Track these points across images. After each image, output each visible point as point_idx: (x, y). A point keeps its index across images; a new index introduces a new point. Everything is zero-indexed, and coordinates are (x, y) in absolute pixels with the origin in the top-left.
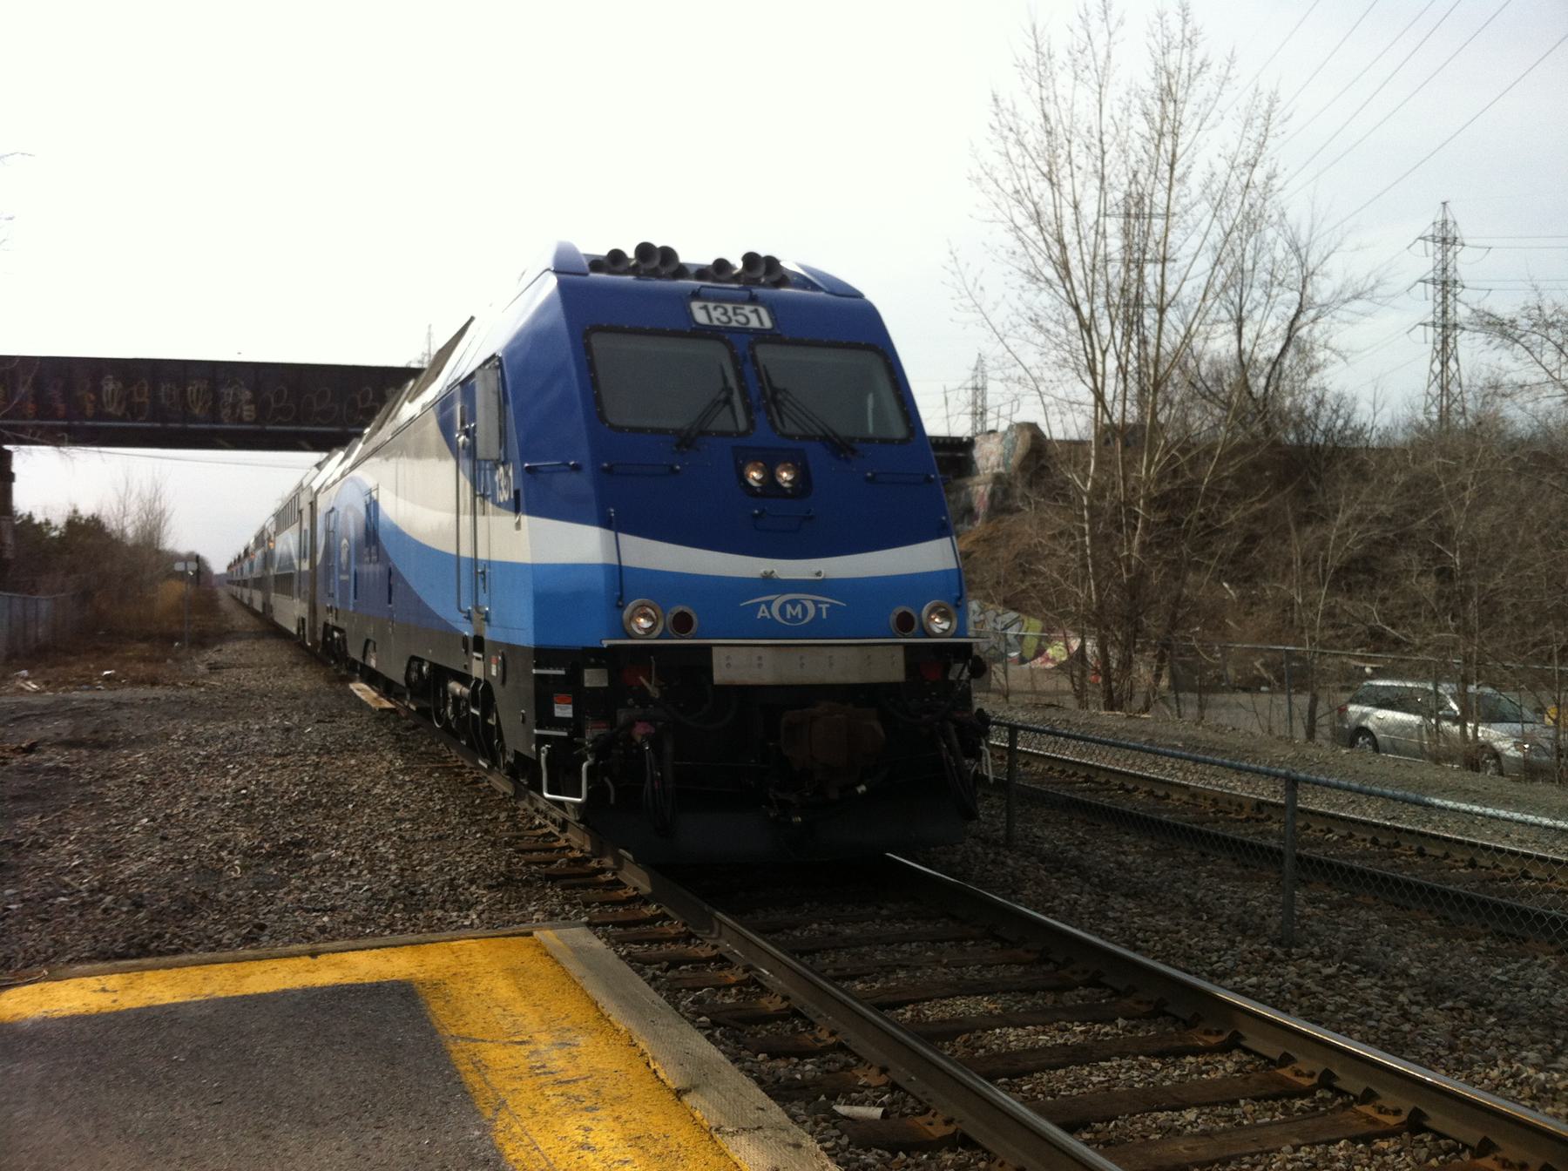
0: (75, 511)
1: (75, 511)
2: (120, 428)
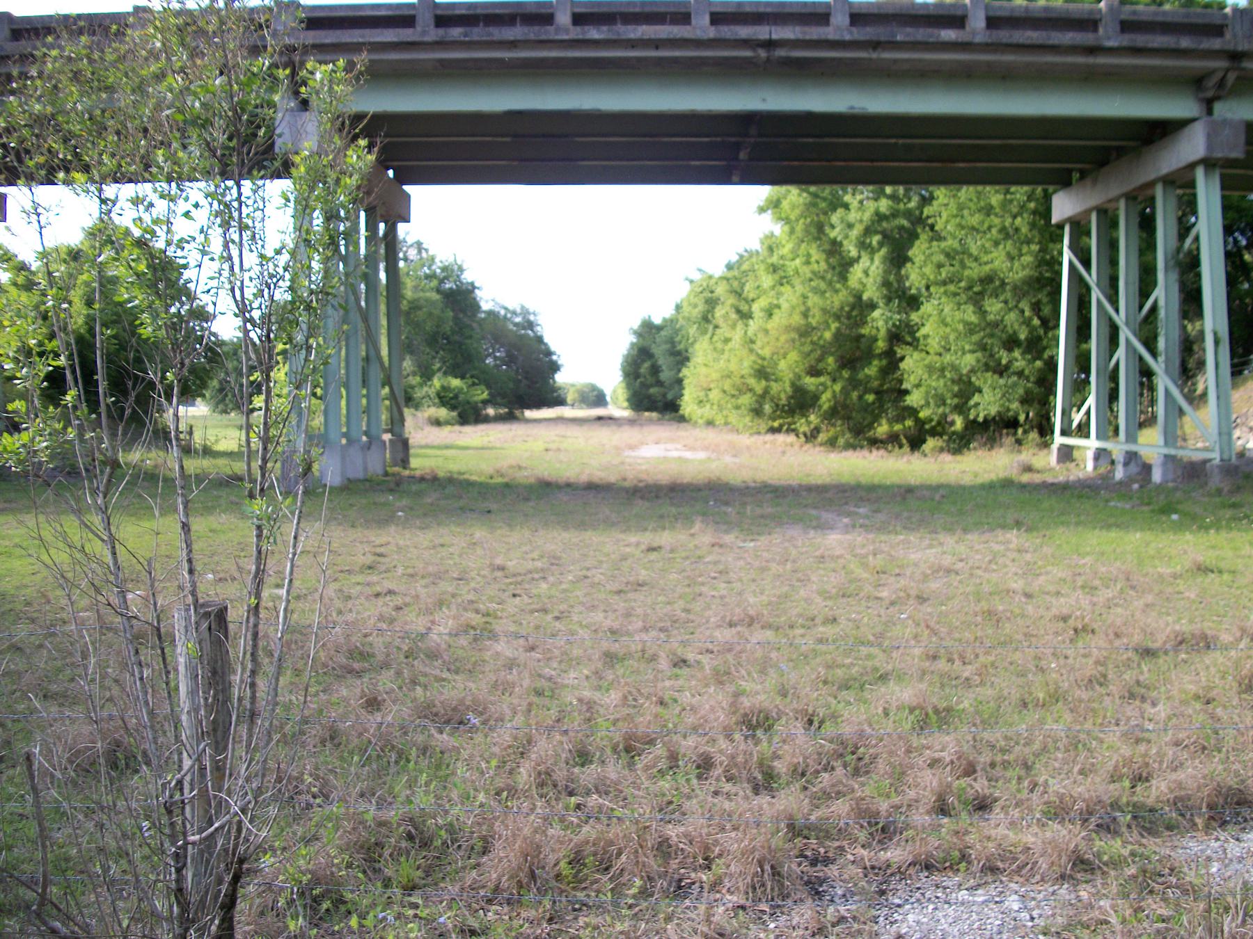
2: (833, 59)
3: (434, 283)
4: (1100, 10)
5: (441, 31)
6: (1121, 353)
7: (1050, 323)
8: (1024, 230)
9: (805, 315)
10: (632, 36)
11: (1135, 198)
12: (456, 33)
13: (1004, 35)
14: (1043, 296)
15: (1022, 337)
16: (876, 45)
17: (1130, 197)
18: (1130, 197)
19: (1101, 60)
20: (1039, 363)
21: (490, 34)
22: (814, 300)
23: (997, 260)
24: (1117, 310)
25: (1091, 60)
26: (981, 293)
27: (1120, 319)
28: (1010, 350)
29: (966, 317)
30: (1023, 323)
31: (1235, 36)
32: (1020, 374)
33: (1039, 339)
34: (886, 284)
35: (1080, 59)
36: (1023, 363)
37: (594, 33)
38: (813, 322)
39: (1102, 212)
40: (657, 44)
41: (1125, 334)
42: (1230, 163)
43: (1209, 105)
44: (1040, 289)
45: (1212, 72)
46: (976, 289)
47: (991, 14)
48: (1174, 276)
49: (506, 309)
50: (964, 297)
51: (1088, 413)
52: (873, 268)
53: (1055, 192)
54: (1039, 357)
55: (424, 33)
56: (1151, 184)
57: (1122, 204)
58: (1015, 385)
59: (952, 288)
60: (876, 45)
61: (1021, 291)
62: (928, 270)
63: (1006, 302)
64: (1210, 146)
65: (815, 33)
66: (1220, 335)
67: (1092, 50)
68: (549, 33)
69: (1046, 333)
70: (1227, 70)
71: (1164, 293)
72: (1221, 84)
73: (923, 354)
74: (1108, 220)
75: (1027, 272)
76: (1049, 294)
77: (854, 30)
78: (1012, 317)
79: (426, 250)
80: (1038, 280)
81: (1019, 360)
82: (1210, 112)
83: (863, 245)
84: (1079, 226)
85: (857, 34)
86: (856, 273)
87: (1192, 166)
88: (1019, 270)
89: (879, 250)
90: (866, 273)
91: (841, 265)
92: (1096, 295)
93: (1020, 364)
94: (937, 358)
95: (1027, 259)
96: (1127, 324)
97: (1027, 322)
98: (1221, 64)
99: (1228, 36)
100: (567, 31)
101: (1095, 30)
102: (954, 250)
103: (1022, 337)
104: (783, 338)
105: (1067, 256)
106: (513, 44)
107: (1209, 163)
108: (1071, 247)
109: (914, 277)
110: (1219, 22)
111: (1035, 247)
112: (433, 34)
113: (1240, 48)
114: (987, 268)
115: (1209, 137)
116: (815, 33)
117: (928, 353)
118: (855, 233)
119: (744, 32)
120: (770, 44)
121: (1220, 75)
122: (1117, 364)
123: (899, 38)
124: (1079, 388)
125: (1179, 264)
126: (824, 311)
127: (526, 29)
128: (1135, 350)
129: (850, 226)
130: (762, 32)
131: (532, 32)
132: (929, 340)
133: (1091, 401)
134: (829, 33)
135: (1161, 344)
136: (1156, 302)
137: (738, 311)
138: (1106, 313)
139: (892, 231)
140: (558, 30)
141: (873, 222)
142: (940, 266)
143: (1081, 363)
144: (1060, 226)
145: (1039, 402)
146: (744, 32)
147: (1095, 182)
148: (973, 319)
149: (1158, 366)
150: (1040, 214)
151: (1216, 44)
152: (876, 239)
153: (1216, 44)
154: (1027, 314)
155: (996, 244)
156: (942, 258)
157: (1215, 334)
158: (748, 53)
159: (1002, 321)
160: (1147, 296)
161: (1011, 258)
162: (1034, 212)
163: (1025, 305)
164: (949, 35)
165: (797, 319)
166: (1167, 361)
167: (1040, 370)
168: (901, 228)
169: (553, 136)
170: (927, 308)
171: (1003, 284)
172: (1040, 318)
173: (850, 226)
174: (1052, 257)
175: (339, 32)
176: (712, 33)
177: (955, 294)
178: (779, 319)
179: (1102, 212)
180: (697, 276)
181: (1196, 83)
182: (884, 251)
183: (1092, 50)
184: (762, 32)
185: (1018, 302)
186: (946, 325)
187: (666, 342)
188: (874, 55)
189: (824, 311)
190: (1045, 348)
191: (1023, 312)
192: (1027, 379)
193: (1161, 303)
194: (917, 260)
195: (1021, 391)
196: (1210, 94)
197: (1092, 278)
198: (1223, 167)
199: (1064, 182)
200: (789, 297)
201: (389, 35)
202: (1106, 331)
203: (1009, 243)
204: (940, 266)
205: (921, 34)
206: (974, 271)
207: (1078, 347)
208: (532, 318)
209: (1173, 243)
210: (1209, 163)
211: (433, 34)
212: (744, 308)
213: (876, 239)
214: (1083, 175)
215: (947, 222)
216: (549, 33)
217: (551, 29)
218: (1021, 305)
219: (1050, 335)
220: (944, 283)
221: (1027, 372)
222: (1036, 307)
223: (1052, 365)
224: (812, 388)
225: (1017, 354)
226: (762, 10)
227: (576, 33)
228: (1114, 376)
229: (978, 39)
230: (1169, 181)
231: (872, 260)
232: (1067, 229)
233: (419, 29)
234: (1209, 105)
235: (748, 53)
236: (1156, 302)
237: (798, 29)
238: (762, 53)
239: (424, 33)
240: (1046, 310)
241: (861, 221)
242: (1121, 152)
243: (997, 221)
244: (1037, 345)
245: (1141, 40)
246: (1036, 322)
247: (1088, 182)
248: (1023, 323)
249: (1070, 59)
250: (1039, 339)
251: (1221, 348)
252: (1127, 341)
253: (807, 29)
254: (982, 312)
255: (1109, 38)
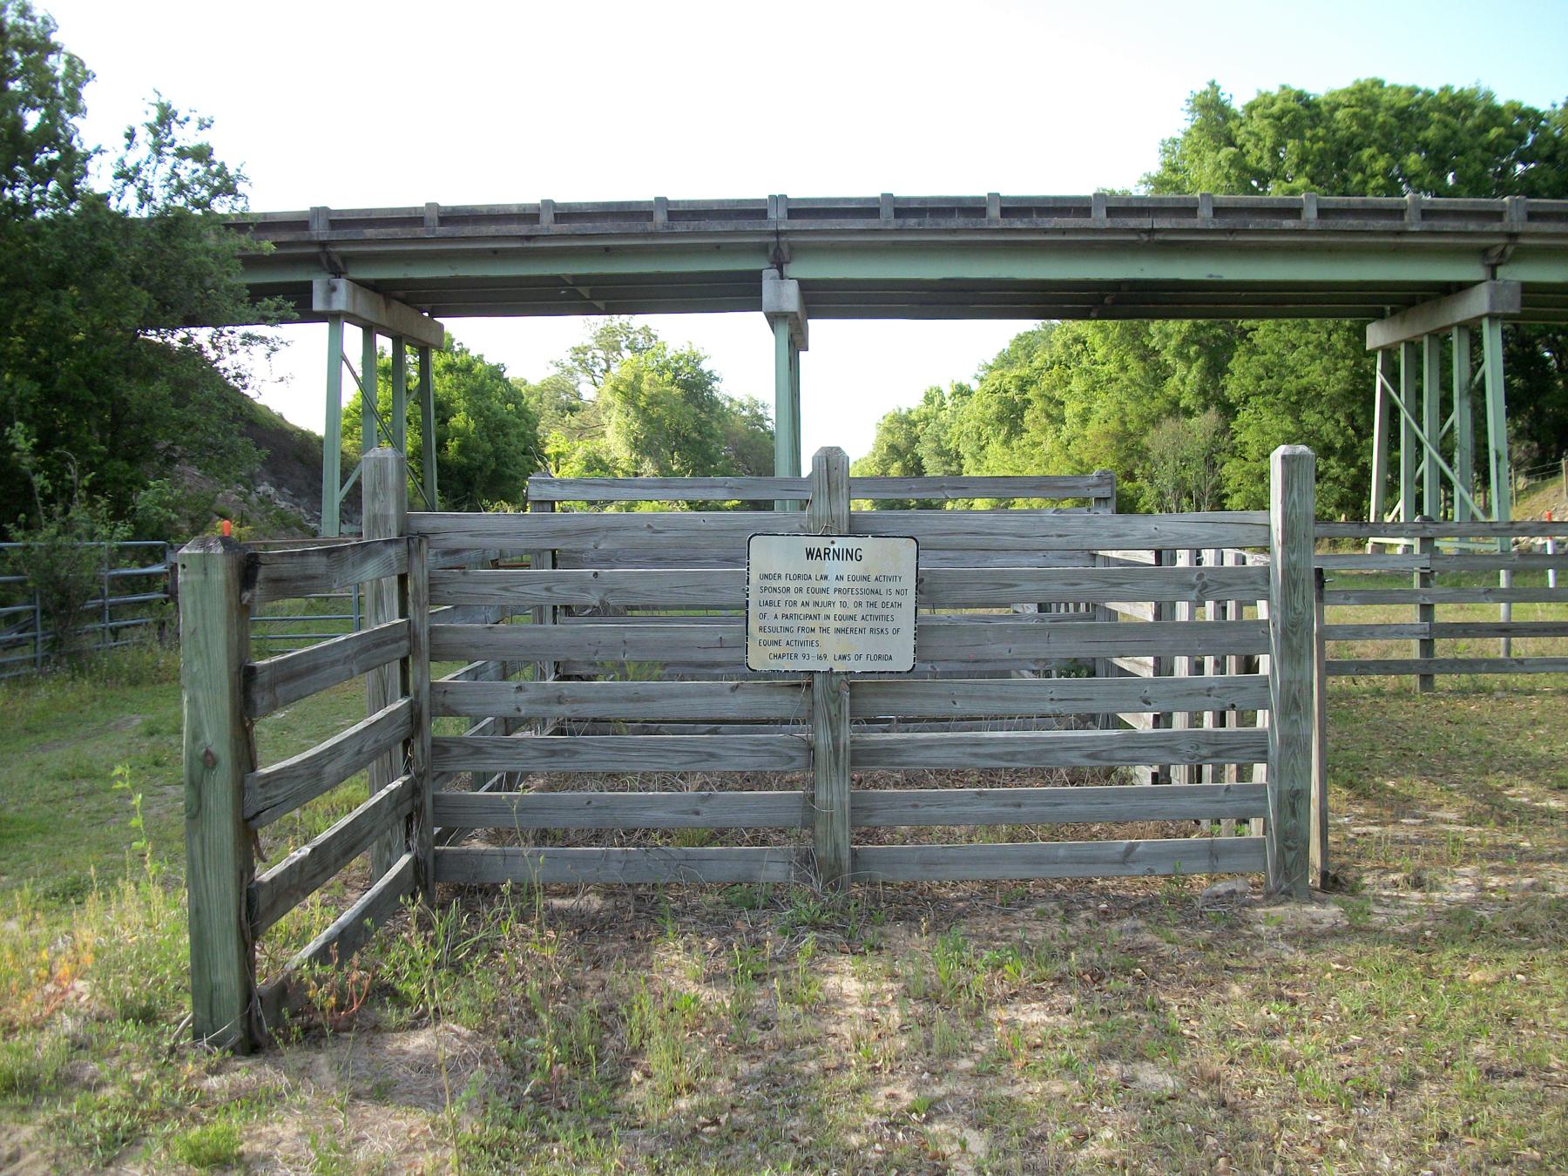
0: (1259, 92)
1: (1259, 92)
3: (669, 376)
4: (1406, 202)
5: (900, 221)
6: (1425, 465)
7: (1364, 433)
8: (1340, 345)
9: (1124, 423)
10: (1047, 226)
11: (1437, 335)
12: (912, 222)
13: (1332, 223)
14: (1356, 408)
15: (1338, 446)
16: (1232, 232)
17: (1433, 335)
18: (1433, 335)
19: (1406, 240)
20: (1353, 471)
21: (938, 224)
22: (1130, 407)
23: (1314, 374)
24: (1422, 430)
25: (1398, 240)
26: (1297, 403)
27: (1424, 437)
28: (1326, 458)
29: (1285, 427)
30: (1339, 433)
31: (1511, 220)
32: (1336, 480)
33: (1354, 446)
34: (1202, 392)
35: (1391, 240)
36: (1339, 470)
37: (1018, 224)
38: (1131, 427)
39: (1410, 344)
40: (1064, 231)
41: (1428, 449)
42: (1506, 317)
43: (1493, 270)
44: (1354, 401)
45: (1495, 246)
46: (1293, 399)
47: (1321, 206)
48: (1467, 403)
49: (731, 400)
50: (1281, 408)
51: (1398, 515)
52: (1191, 377)
53: (1370, 322)
54: (1353, 465)
55: (887, 223)
56: (1450, 327)
57: (1426, 340)
58: (1330, 489)
59: (1270, 398)
60: (1232, 232)
61: (1335, 403)
62: (1248, 382)
63: (1322, 413)
64: (1492, 304)
65: (1187, 223)
66: (1501, 453)
67: (1399, 233)
68: (984, 223)
69: (1359, 441)
70: (1506, 245)
71: (1460, 417)
72: (1502, 254)
73: (1242, 461)
74: (1414, 347)
75: (1342, 385)
76: (1364, 404)
77: (1216, 220)
78: (1328, 428)
79: (656, 337)
80: (1352, 393)
81: (1335, 467)
82: (1494, 277)
83: (1180, 354)
84: (1389, 352)
85: (1219, 224)
86: (1173, 382)
87: (1480, 318)
88: (1336, 384)
89: (1197, 359)
90: (1183, 381)
91: (1159, 375)
92: (1404, 415)
93: (1335, 471)
94: (1254, 464)
95: (1342, 373)
96: (1430, 441)
97: (1343, 432)
98: (1502, 241)
99: (1506, 219)
100: (997, 222)
101: (1402, 218)
102: (1273, 363)
103: (1338, 446)
104: (1102, 444)
105: (1379, 378)
106: (954, 231)
107: (1492, 317)
108: (1382, 372)
109: (1233, 388)
110: (1499, 209)
111: (1349, 363)
112: (895, 223)
113: (1515, 230)
114: (1304, 381)
115: (1492, 297)
116: (1187, 223)
117: (1245, 459)
118: (1173, 343)
119: (1133, 222)
120: (1152, 231)
121: (1500, 248)
122: (1422, 475)
123: (1251, 227)
124: (1391, 489)
125: (1470, 392)
126: (1141, 417)
127: (966, 220)
128: (1437, 463)
129: (1168, 336)
130: (1146, 222)
131: (971, 222)
132: (1248, 447)
133: (1400, 505)
134: (1197, 223)
135: (1456, 460)
136: (1452, 425)
137: (1049, 416)
138: (1413, 430)
139: (1208, 340)
140: (990, 221)
141: (1191, 332)
142: (1260, 378)
143: (1392, 466)
144: (1373, 353)
145: (1354, 506)
146: (1133, 222)
147: (1403, 321)
148: (1291, 428)
149: (1454, 476)
150: (1354, 330)
151: (1497, 227)
152: (1193, 349)
153: (1497, 227)
154: (1342, 424)
155: (1313, 358)
156: (1261, 371)
157: (1497, 452)
158: (1134, 238)
159: (1319, 430)
160: (1447, 417)
161: (1327, 372)
162: (1349, 329)
163: (1340, 416)
164: (1289, 223)
165: (1113, 425)
166: (1461, 472)
167: (1354, 476)
168: (1216, 337)
169: (962, 290)
170: (1243, 417)
171: (1319, 395)
172: (1353, 428)
173: (1168, 336)
174: (1366, 371)
175: (820, 221)
176: (1108, 223)
177: (1272, 405)
178: (1093, 428)
179: (1410, 344)
180: (174, 108)
181: (1484, 252)
182: (1201, 361)
183: (1399, 233)
184: (1146, 222)
185: (1334, 412)
186: (1265, 433)
187: (933, 440)
188: (1231, 239)
189: (1141, 417)
190: (1359, 456)
191: (1338, 422)
192: (1342, 484)
193: (1457, 425)
194: (1236, 373)
195: (1336, 496)
196: (1494, 261)
197: (1401, 401)
198: (1287, 684)
199: (1379, 316)
200: (1103, 405)
201: (860, 224)
202: (1412, 443)
203: (1326, 357)
204: (1260, 378)
205: (1267, 223)
206: (1291, 384)
207: (1389, 455)
208: (760, 411)
209: (1466, 375)
210: (1492, 317)
211: (895, 223)
212: (1055, 412)
213: (1193, 349)
214: (1393, 312)
215: (1266, 336)
216: (984, 223)
217: (985, 220)
218: (1336, 416)
219: (1364, 443)
220: (1263, 393)
221: (1342, 478)
222: (1351, 418)
223: (1365, 471)
224: (1131, 493)
225: (1332, 461)
226: (1145, 205)
227: (1004, 223)
228: (1420, 482)
229: (1311, 227)
230: (1462, 326)
231: (1189, 368)
232: (1379, 355)
233: (883, 219)
234: (1493, 270)
235: (1134, 238)
236: (1452, 425)
237: (1173, 220)
238: (1145, 238)
239: (887, 223)
240: (1360, 421)
241: (1179, 332)
242: (1425, 299)
243: (1314, 337)
244: (1352, 454)
245: (1438, 224)
246: (1350, 432)
247: (1398, 317)
248: (1339, 433)
249: (1382, 240)
250: (1354, 446)
251: (1501, 464)
252: (1430, 454)
253: (1180, 220)
254: (1298, 421)
255: (1412, 224)
